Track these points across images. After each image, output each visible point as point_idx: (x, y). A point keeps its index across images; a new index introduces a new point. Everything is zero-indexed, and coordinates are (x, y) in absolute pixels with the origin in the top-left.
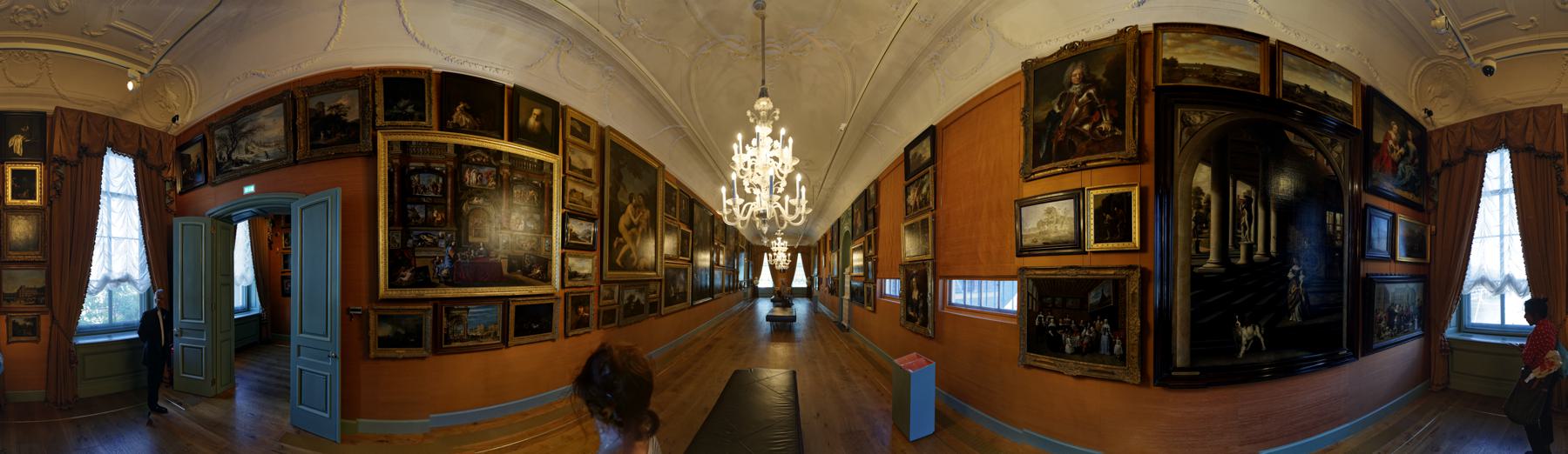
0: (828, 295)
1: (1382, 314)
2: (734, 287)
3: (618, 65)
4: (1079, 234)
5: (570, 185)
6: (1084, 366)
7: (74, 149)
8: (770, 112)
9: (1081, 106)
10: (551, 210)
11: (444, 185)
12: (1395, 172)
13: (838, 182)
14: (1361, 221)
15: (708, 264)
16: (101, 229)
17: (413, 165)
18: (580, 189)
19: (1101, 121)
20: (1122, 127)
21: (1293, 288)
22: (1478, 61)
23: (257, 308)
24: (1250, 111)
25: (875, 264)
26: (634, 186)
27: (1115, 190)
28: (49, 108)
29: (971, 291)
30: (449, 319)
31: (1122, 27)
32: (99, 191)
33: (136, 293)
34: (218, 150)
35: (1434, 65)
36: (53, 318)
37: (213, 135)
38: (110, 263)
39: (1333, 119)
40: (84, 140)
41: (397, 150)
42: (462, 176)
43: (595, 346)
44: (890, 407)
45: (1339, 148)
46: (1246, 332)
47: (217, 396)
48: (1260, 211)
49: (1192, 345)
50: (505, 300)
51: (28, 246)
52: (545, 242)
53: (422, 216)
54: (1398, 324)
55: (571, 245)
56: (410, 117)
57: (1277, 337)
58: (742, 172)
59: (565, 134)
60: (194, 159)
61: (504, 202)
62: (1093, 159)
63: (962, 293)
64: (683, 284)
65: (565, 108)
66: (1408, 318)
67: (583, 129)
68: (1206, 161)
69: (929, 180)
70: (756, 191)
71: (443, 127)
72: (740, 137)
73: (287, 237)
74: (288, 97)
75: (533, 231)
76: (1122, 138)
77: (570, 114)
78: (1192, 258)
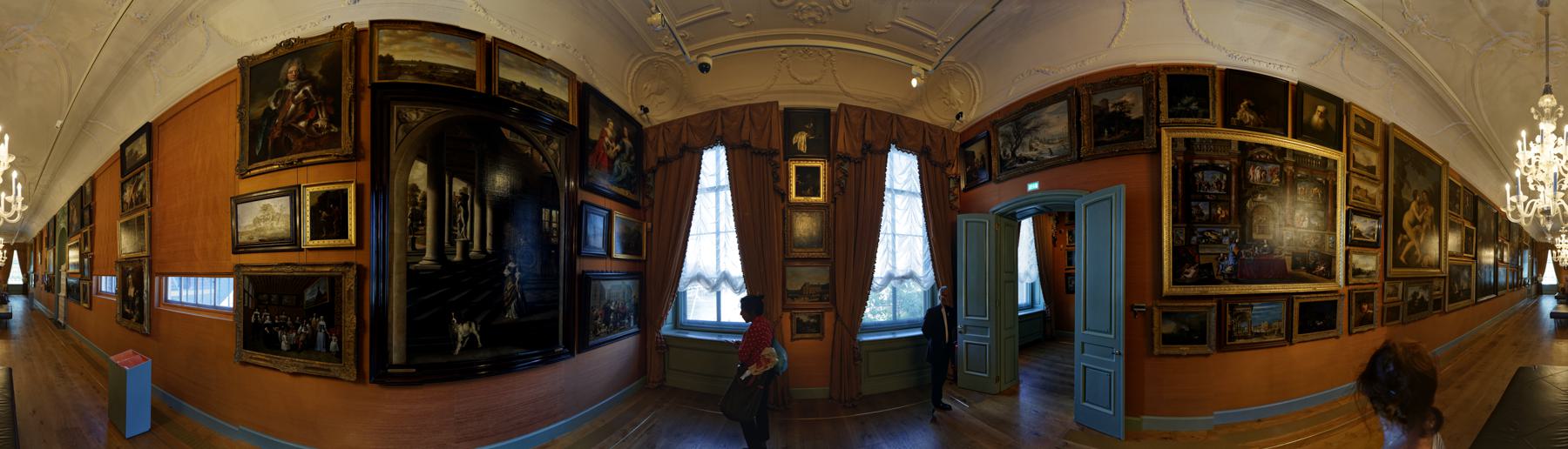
0: (44, 292)
1: (597, 311)
2: (1518, 284)
3: (1404, 64)
4: (296, 231)
5: (1354, 182)
6: (300, 363)
7: (858, 146)
8: (1553, 109)
9: (297, 103)
10: (1335, 207)
11: (1228, 182)
12: (611, 169)
13: (54, 178)
14: (577, 218)
15: (1492, 261)
16: (885, 226)
17: (1197, 162)
18: (1364, 186)
19: (317, 118)
20: (339, 125)
21: (509, 285)
22: (693, 58)
23: (1041, 305)
24: (468, 109)
25: (91, 261)
26: (1417, 183)
27: (331, 187)
28: (833, 105)
29: (187, 288)
30: (1233, 316)
31: (338, 24)
32: (883, 188)
33: (920, 290)
34: (1002, 146)
35: (650, 62)
36: (837, 315)
37: (997, 132)
38: (894, 259)
39: (549, 116)
40: (867, 137)
41: (1181, 147)
42: (1246, 173)
43: (1379, 343)
44: (106, 404)
45: (555, 145)
46: (462, 329)
47: (1001, 393)
48: (477, 209)
49: (408, 342)
50: (1289, 297)
51: (812, 243)
52: (1329, 239)
53: (1206, 213)
54: (614, 321)
55: (1355, 242)
56: (1194, 114)
57: (493, 334)
58: (1526, 169)
59: (1349, 131)
60: (978, 156)
61: (1289, 199)
62: (310, 156)
63: (179, 290)
64: (1467, 282)
65: (1349, 105)
66: (624, 315)
67: (1367, 126)
68: (422, 158)
69: (145, 177)
70: (1540, 188)
71: (1227, 124)
72: (1524, 134)
73: (1071, 234)
74: (1073, 94)
75: (1317, 228)
76: (338, 134)
77: (1354, 111)
78: (408, 254)
